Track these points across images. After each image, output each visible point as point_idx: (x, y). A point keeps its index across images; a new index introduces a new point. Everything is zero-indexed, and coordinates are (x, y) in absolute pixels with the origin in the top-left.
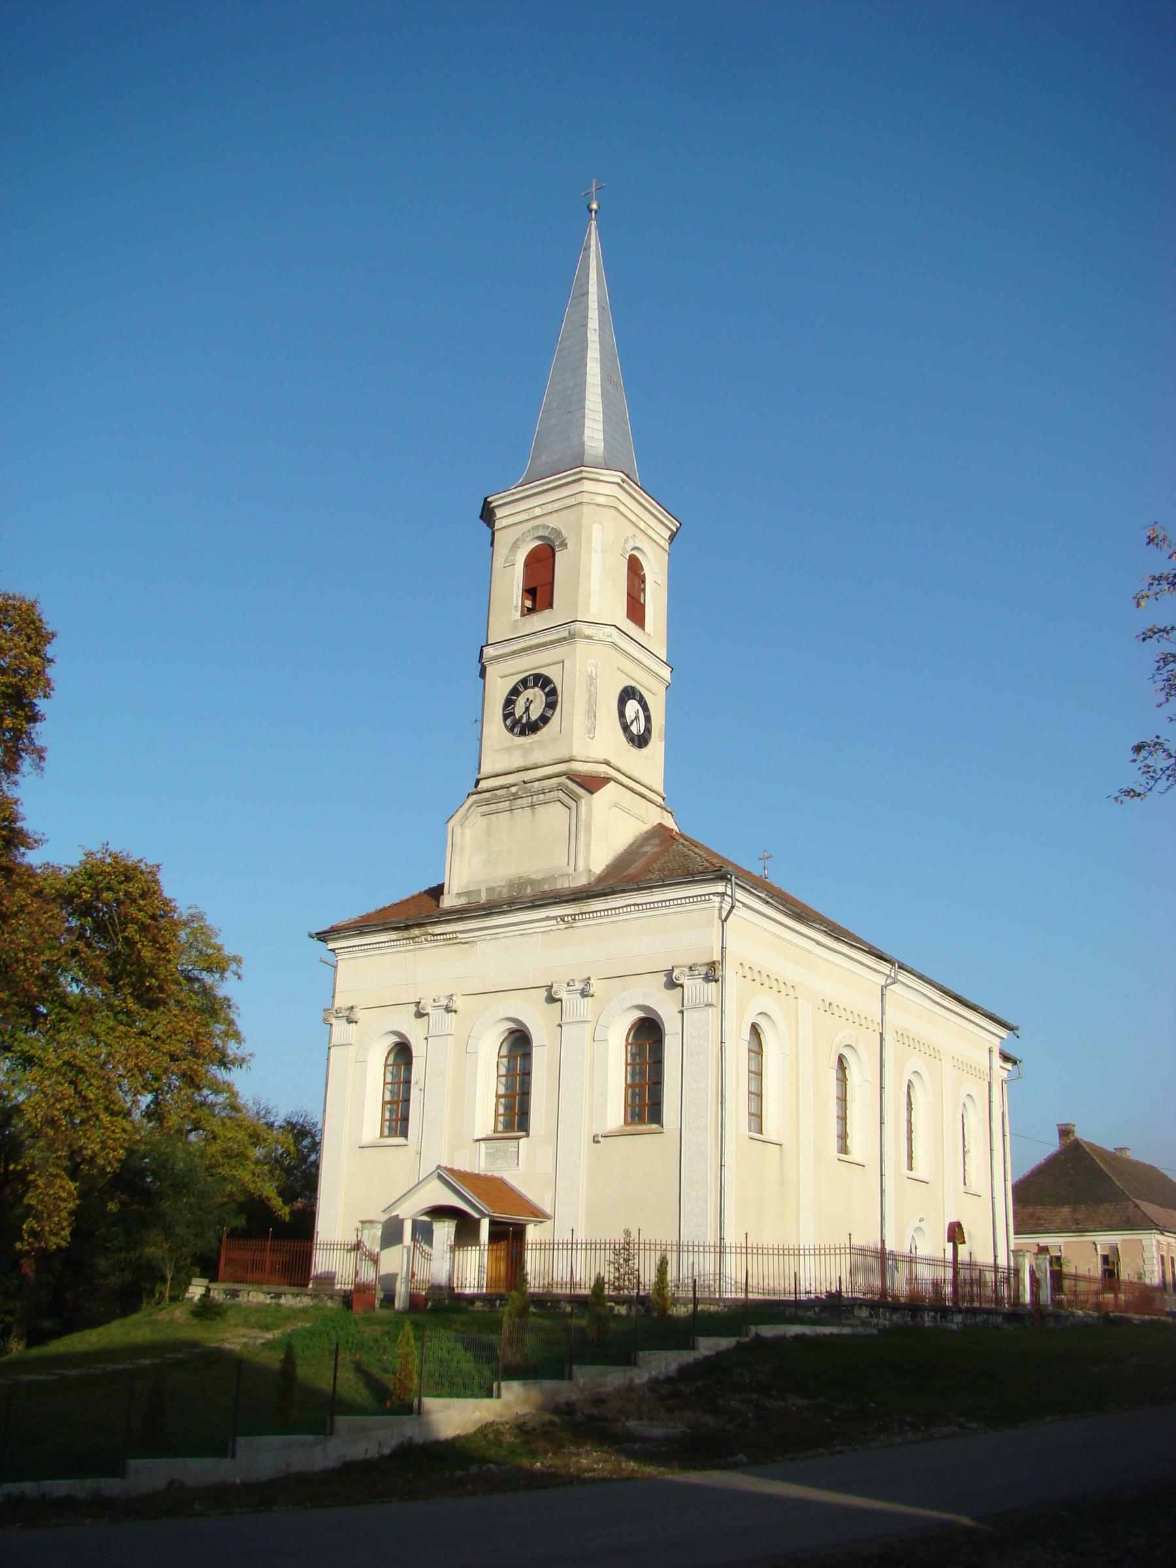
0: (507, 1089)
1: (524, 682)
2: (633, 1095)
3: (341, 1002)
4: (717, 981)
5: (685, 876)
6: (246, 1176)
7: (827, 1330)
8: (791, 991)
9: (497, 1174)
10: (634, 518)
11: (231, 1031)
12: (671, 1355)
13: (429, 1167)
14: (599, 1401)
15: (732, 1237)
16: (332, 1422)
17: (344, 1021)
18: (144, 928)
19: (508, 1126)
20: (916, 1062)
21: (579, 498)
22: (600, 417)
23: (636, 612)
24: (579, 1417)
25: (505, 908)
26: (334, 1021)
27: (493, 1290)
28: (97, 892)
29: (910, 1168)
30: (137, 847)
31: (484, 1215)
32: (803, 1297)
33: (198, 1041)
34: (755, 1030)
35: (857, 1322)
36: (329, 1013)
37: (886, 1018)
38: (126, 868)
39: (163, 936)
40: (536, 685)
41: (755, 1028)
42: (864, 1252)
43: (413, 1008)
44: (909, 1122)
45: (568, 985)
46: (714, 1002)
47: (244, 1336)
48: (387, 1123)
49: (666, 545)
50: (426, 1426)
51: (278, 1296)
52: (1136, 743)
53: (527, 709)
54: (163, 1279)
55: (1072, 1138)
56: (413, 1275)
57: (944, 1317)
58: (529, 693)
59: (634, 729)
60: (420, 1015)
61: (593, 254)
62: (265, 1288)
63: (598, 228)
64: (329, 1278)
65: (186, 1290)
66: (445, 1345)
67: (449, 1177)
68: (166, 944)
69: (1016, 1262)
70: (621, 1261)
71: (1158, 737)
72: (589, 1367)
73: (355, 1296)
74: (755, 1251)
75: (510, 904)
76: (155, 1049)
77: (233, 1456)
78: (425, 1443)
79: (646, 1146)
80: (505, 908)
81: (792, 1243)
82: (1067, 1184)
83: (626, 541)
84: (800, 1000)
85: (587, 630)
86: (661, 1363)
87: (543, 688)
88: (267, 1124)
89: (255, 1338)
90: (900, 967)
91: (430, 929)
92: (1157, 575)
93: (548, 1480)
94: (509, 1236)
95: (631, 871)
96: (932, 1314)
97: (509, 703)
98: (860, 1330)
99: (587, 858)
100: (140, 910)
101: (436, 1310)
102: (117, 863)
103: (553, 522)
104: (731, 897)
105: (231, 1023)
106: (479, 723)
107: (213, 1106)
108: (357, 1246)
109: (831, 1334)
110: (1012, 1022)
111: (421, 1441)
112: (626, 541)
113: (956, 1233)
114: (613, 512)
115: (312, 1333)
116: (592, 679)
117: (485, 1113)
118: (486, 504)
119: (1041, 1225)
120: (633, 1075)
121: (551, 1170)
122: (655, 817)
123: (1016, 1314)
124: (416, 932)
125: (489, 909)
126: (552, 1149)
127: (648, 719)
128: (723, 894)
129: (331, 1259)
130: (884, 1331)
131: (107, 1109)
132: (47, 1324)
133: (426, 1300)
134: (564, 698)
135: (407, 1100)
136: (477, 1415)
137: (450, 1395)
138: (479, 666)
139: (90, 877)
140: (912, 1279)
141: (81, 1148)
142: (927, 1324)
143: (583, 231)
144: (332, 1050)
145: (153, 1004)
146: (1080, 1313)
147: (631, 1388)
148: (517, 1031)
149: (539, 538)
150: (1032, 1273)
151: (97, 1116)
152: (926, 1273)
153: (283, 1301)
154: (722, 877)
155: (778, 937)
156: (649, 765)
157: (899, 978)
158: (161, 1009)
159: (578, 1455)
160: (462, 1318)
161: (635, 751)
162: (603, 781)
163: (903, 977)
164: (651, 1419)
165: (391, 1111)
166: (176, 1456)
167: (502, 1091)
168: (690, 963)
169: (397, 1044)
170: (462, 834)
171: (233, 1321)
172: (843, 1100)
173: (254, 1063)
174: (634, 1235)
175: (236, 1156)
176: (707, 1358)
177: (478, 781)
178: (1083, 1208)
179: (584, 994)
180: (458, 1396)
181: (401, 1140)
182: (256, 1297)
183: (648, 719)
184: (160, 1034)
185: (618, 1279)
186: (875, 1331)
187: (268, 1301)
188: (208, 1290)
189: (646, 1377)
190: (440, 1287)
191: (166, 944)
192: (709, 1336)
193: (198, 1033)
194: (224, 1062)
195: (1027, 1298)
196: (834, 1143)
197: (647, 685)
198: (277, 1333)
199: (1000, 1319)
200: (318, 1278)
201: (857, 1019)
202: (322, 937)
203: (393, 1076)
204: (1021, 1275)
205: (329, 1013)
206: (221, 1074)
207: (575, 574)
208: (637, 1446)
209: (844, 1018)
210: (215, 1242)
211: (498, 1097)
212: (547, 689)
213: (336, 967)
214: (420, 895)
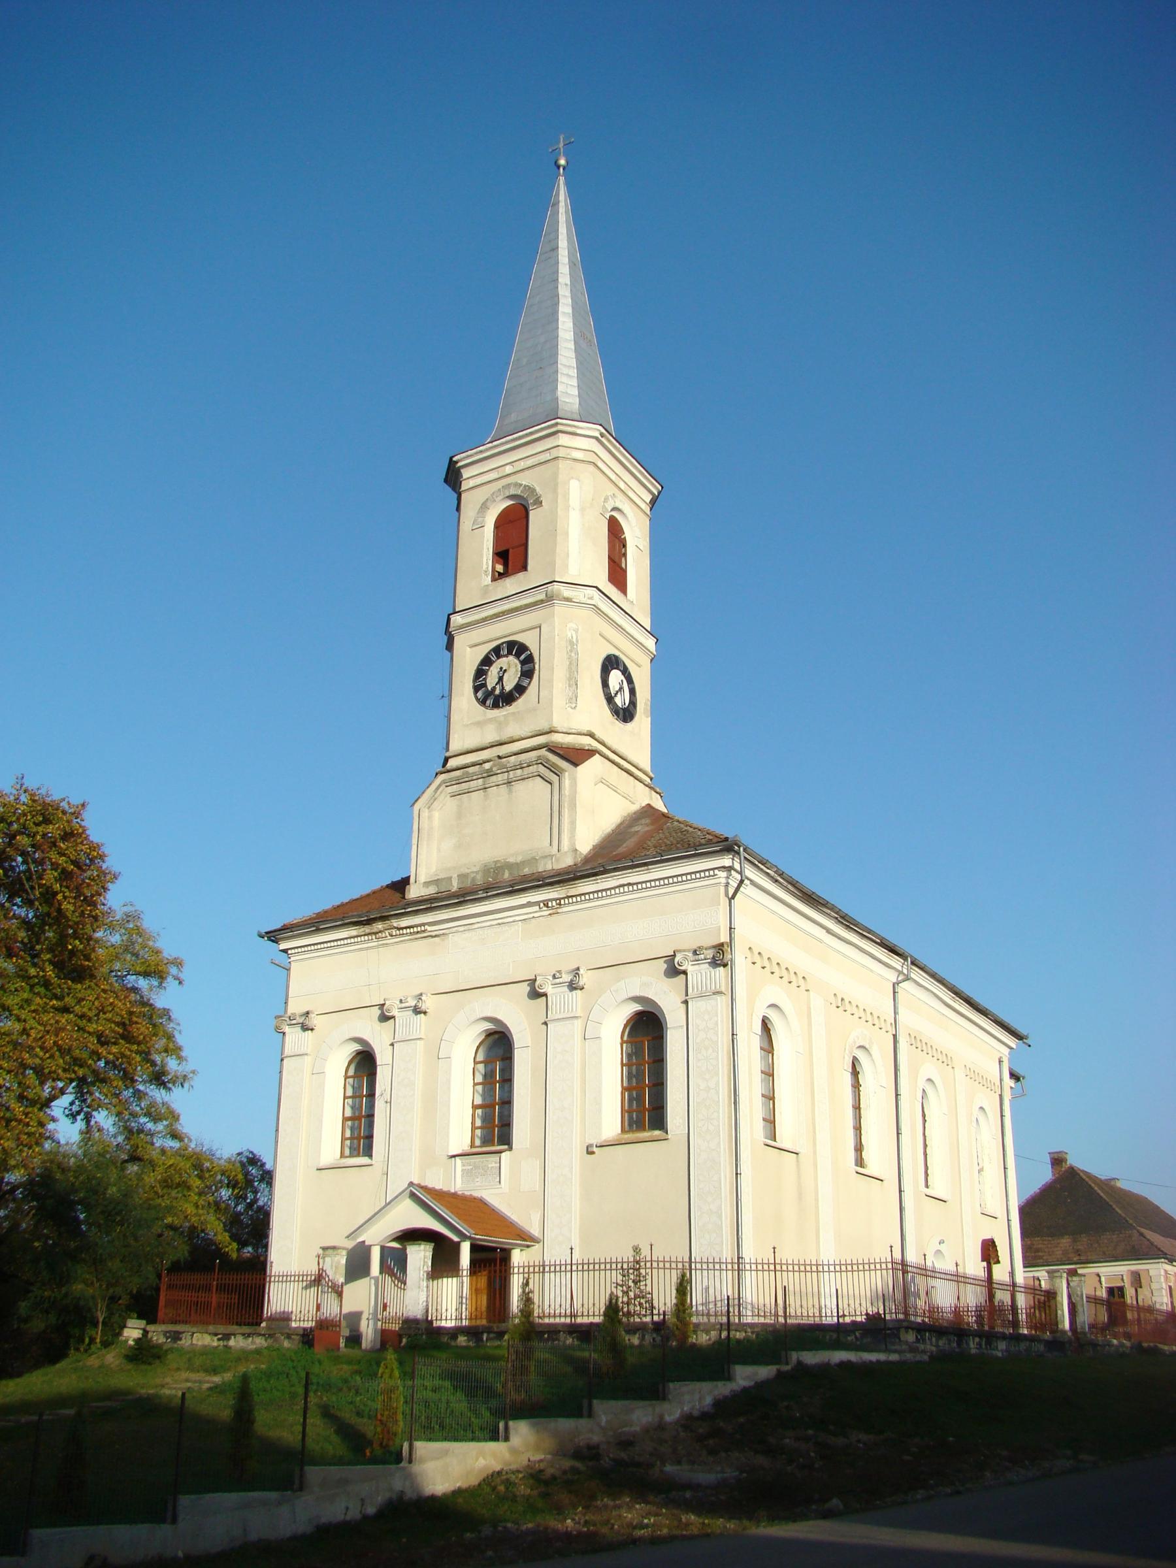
1: (497, 651)
2: (630, 1100)
3: (295, 1007)
4: (725, 965)
6: (190, 1209)
7: (873, 1357)
8: (801, 982)
9: (476, 1194)
10: (613, 477)
11: (171, 1045)
12: (706, 1386)
13: (398, 1184)
14: (626, 1443)
18: (65, 876)
19: (487, 1141)
20: (929, 1068)
21: (554, 453)
22: (574, 372)
23: (618, 576)
24: (606, 1462)
26: (287, 1029)
27: (473, 1323)
29: (927, 1186)
30: (59, 788)
33: (132, 1023)
35: (904, 1347)
36: (281, 1021)
37: (900, 1017)
38: (45, 805)
40: (510, 653)
41: (765, 1023)
43: (376, 1012)
45: (554, 977)
46: (723, 989)
47: (187, 1380)
48: (348, 1142)
50: (409, 1477)
51: (227, 1337)
53: (501, 679)
56: (385, 1306)
57: (989, 1343)
58: (503, 662)
59: (618, 701)
60: (385, 1018)
61: (562, 210)
62: (211, 1328)
63: (567, 184)
64: (285, 1318)
65: (120, 1334)
67: (420, 1195)
70: (631, 1284)
72: (612, 1403)
73: (316, 1333)
75: (486, 890)
76: (80, 1029)
77: (174, 1521)
79: (649, 1155)
82: (1068, 1211)
83: (606, 500)
84: (811, 993)
85: (567, 592)
86: (693, 1397)
87: (518, 656)
89: (200, 1382)
90: (913, 963)
91: (395, 923)
93: (588, 1543)
94: (492, 1263)
95: (621, 850)
96: (977, 1340)
97: (480, 673)
98: (909, 1356)
102: (34, 801)
103: (525, 479)
104: (740, 873)
105: (170, 1037)
106: (446, 700)
108: (318, 1280)
109: (878, 1361)
110: (1022, 1031)
112: (606, 500)
114: (592, 468)
115: (268, 1375)
117: (460, 1127)
118: (452, 464)
119: (1041, 1258)
120: (630, 1076)
121: (538, 1187)
122: (644, 797)
124: (379, 926)
125: (464, 896)
126: (538, 1164)
127: (632, 692)
128: (729, 869)
129: (287, 1299)
131: (21, 1098)
133: (400, 1336)
135: (371, 1116)
136: (482, 1462)
138: (446, 638)
142: (973, 1351)
143: (547, 202)
147: (661, 1426)
148: (496, 1032)
149: (511, 497)
153: (232, 1343)
155: (788, 921)
156: (635, 740)
157: (913, 976)
161: (619, 725)
162: (590, 753)
163: (916, 974)
164: (693, 1463)
165: (352, 1129)
166: (99, 1522)
168: (695, 947)
169: (359, 1053)
170: (430, 818)
171: (175, 1365)
173: (196, 1081)
174: (645, 1252)
175: (178, 1185)
176: (745, 1390)
177: (446, 760)
178: (1084, 1239)
179: (572, 986)
180: (456, 1439)
181: (364, 1160)
182: (201, 1339)
183: (632, 692)
186: (926, 1358)
187: (215, 1344)
188: (146, 1332)
189: (677, 1414)
190: (415, 1321)
191: (92, 896)
193: (131, 1013)
194: (159, 1078)
195: (1067, 1325)
196: (851, 1155)
197: (634, 657)
198: (228, 1376)
199: (1042, 1348)
200: (271, 1319)
201: (869, 1018)
202: (273, 936)
205: (281, 1021)
206: (157, 1094)
207: (552, 533)
208: (688, 1494)
209: (863, 1019)
210: (152, 1277)
211: (475, 1107)
212: (523, 657)
213: (288, 970)
214: (382, 889)
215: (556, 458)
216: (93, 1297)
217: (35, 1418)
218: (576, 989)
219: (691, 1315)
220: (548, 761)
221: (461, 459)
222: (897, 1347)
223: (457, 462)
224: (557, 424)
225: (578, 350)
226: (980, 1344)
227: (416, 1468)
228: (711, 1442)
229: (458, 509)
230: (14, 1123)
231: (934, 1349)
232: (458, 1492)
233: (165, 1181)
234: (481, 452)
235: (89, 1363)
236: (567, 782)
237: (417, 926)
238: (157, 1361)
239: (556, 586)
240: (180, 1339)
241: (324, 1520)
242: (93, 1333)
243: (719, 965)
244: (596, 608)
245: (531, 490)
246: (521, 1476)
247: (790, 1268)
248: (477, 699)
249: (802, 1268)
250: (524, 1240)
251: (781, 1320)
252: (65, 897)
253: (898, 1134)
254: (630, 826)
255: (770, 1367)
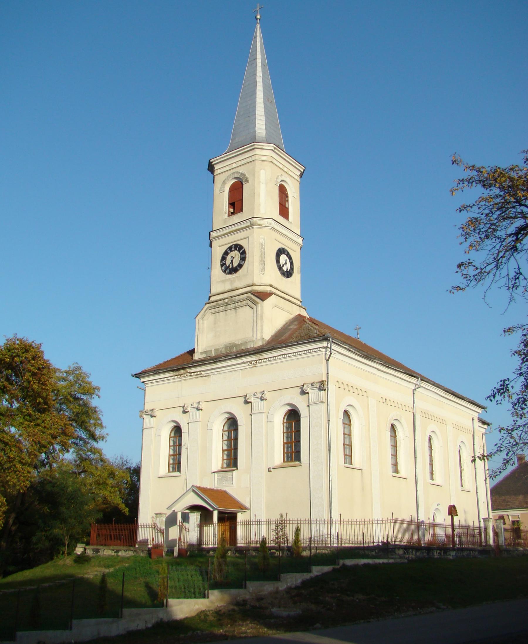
0: (228, 446)
1: (230, 248)
2: (287, 448)
3: (148, 407)
4: (325, 390)
5: (307, 339)
7: (381, 561)
9: (223, 489)
10: (281, 166)
13: (189, 486)
14: (260, 599)
15: (335, 517)
16: (122, 611)
17: (149, 416)
18: (34, 374)
19: (229, 465)
20: (432, 426)
22: (263, 118)
23: (284, 211)
25: (223, 358)
26: (145, 416)
28: (12, 358)
30: (31, 336)
31: (215, 509)
32: (366, 545)
33: (66, 428)
34: (346, 413)
35: (397, 556)
36: (142, 413)
38: (26, 345)
39: (43, 378)
40: (236, 249)
42: (408, 523)
43: (181, 409)
44: (431, 456)
46: (324, 401)
48: (172, 466)
49: (298, 179)
50: (168, 613)
51: (118, 551)
52: (460, 262)
53: (232, 261)
54: (64, 545)
55: (523, 461)
59: (284, 268)
60: (185, 412)
61: (258, 40)
62: (111, 547)
63: (261, 27)
64: (145, 542)
65: (75, 550)
66: (191, 574)
67: (200, 491)
68: (45, 381)
69: (485, 524)
70: (279, 529)
71: (469, 260)
74: (315, 522)
75: (225, 356)
77: (71, 629)
78: (168, 621)
79: (294, 472)
80: (223, 358)
81: (369, 518)
83: (277, 177)
84: (369, 398)
85: (259, 222)
86: (292, 580)
87: (239, 251)
88: (127, 468)
90: (422, 380)
91: (188, 370)
92: (461, 179)
93: (224, 637)
94: (229, 519)
95: (283, 338)
96: (438, 551)
97: (223, 258)
98: (399, 560)
99: (262, 333)
100: (32, 366)
101: (191, 556)
102: (21, 343)
103: (241, 170)
104: (330, 348)
107: (90, 460)
109: (383, 563)
111: (166, 620)
112: (277, 177)
113: (452, 511)
114: (270, 163)
116: (262, 246)
117: (217, 458)
119: (509, 505)
120: (287, 438)
121: (249, 486)
122: (296, 311)
123: (485, 550)
124: (182, 372)
126: (249, 476)
127: (292, 263)
128: (326, 348)
129: (144, 534)
130: (411, 561)
131: (20, 462)
132: (11, 568)
134: (249, 255)
135: (180, 454)
136: (197, 607)
137: (184, 598)
139: (9, 351)
140: (434, 535)
141: (8, 481)
142: (436, 557)
144: (144, 431)
145: (42, 411)
146: (521, 549)
147: (277, 592)
148: (231, 418)
149: (236, 178)
150: (494, 529)
151: (15, 465)
152: (441, 531)
153: (120, 554)
154: (326, 339)
156: (293, 286)
157: (421, 385)
158: (47, 413)
159: (242, 625)
160: (201, 560)
161: (285, 279)
162: (270, 294)
163: (424, 384)
165: (173, 459)
167: (225, 448)
168: (312, 382)
169: (175, 427)
170: (203, 323)
172: (395, 446)
173: (108, 438)
174: (285, 517)
175: (102, 484)
176: (317, 576)
177: (210, 297)
179: (262, 399)
180: (188, 598)
181: (177, 474)
182: (107, 552)
184: (46, 425)
185: (278, 538)
186: (406, 561)
187: (113, 554)
188: (85, 549)
189: (285, 586)
191: (45, 381)
192: (318, 565)
193: (65, 424)
195: (491, 542)
196: (390, 468)
199: (476, 553)
201: (400, 406)
202: (138, 376)
203: (174, 442)
204: (488, 531)
205: (142, 413)
207: (253, 195)
208: (272, 621)
209: (397, 407)
211: (223, 451)
212: (241, 251)
213: (145, 390)
214: (185, 354)
215: (254, 160)
216: (63, 535)
217: (36, 587)
218: (263, 400)
219: (301, 543)
220: (251, 298)
221: (214, 161)
222: (394, 556)
223: (212, 162)
224: (254, 145)
225: (265, 108)
226: (440, 553)
227: (169, 609)
228: (296, 598)
229: (214, 183)
230: (18, 472)
231: (414, 556)
232: (186, 618)
233: (96, 482)
234: (222, 158)
235: (59, 563)
236: (259, 308)
237: (197, 372)
238: (86, 563)
239: (255, 219)
240: (99, 552)
241: (131, 629)
242: (64, 549)
243: (322, 390)
244: (273, 228)
245: (243, 175)
246: (211, 612)
247: (347, 523)
248: (222, 270)
249: (355, 523)
250: (242, 509)
251: (340, 545)
252: (34, 383)
253: (415, 457)
254: (289, 325)
255: (329, 567)
